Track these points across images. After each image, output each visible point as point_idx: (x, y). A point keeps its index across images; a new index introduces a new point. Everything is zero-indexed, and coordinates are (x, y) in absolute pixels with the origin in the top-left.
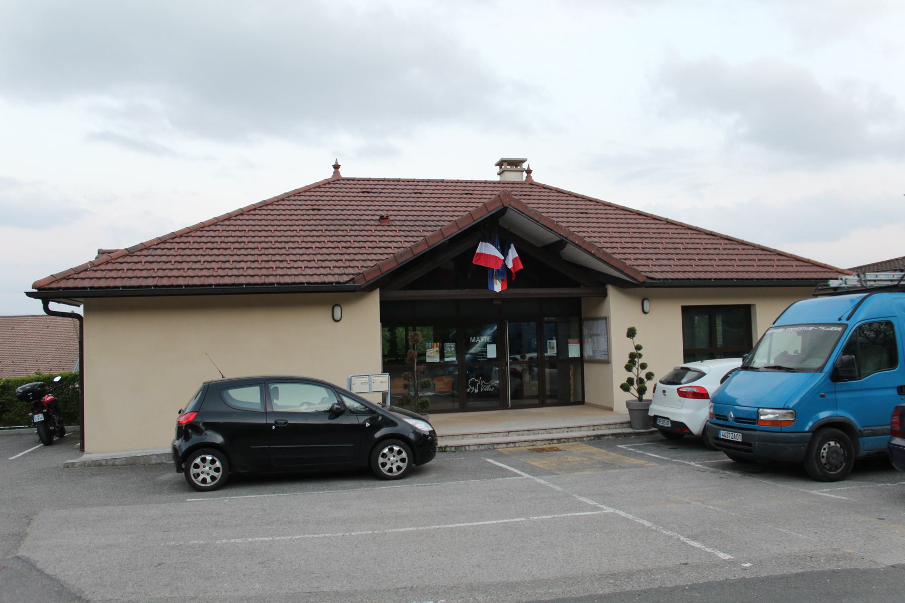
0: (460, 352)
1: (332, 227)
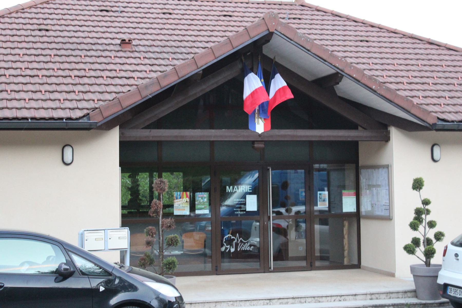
0: (214, 204)
1: (62, 52)
